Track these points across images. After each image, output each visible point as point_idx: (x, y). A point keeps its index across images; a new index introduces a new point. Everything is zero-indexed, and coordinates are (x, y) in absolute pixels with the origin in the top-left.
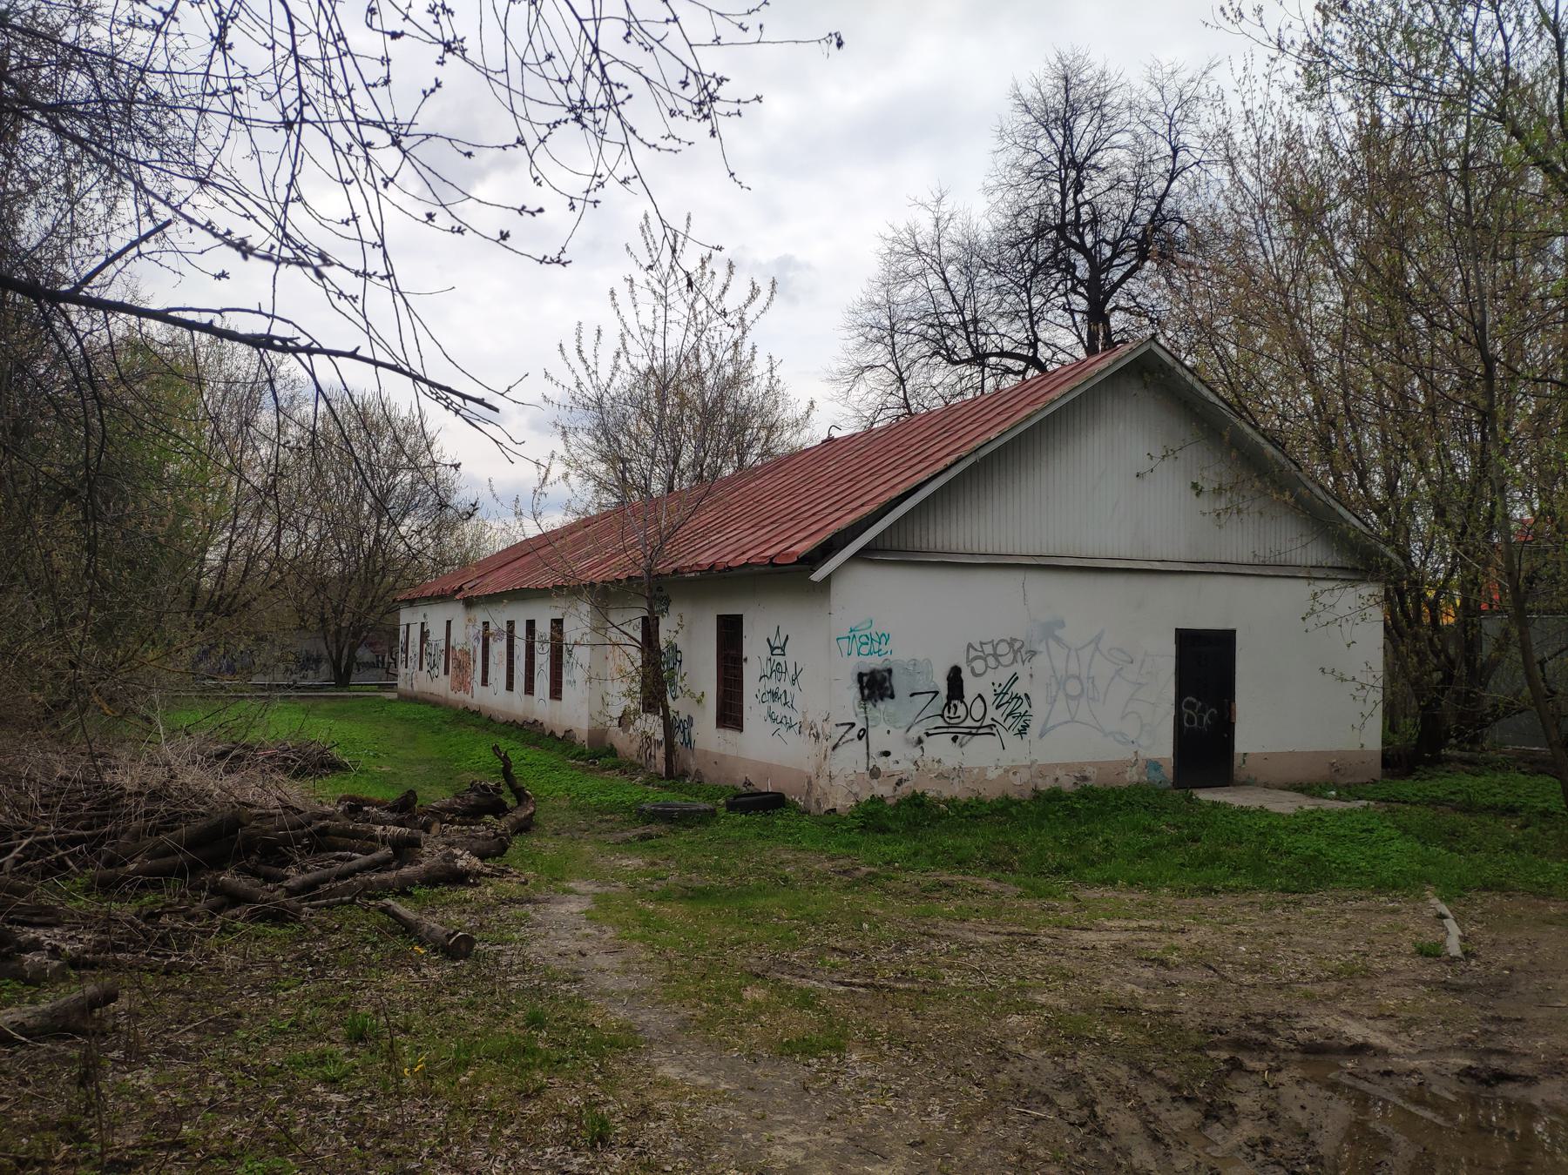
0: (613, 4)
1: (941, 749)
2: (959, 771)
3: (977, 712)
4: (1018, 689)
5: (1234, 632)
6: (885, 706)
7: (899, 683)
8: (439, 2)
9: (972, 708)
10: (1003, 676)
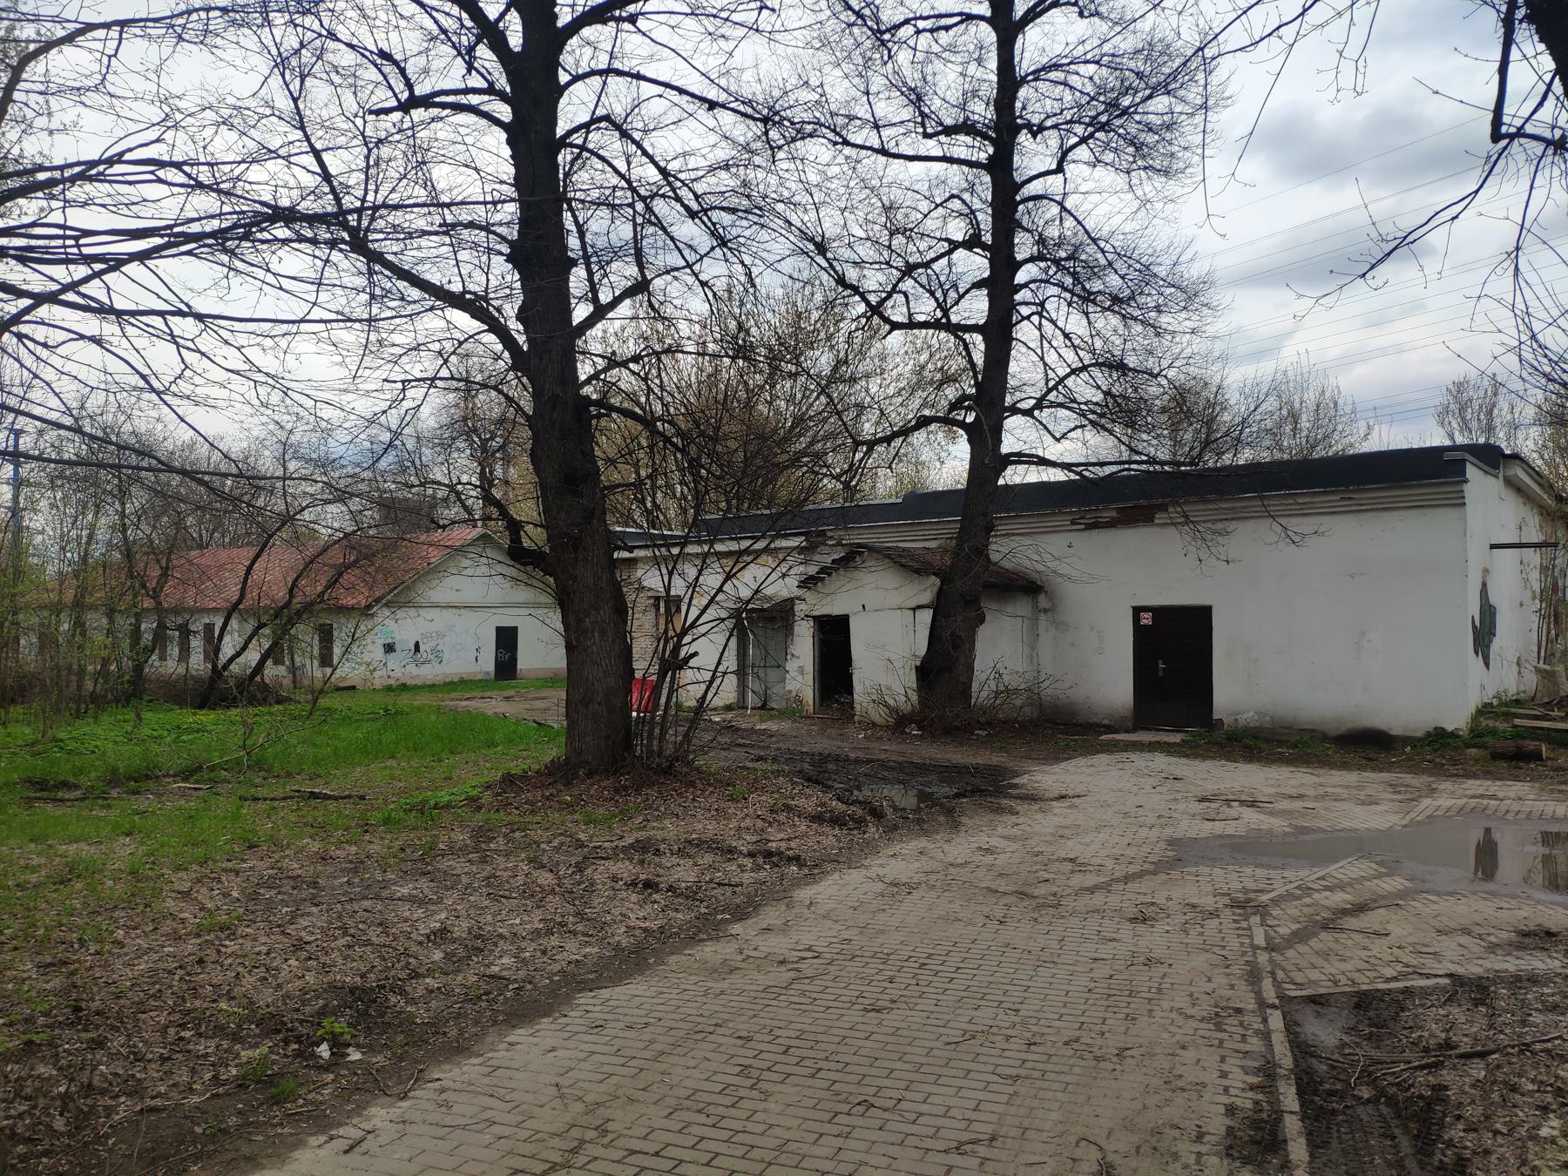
0: (1495, 1174)
1: (412, 669)
2: (418, 676)
3: (425, 656)
4: (439, 648)
5: (498, 629)
6: (393, 654)
7: (397, 647)
8: (876, 3)
9: (423, 654)
10: (434, 644)
